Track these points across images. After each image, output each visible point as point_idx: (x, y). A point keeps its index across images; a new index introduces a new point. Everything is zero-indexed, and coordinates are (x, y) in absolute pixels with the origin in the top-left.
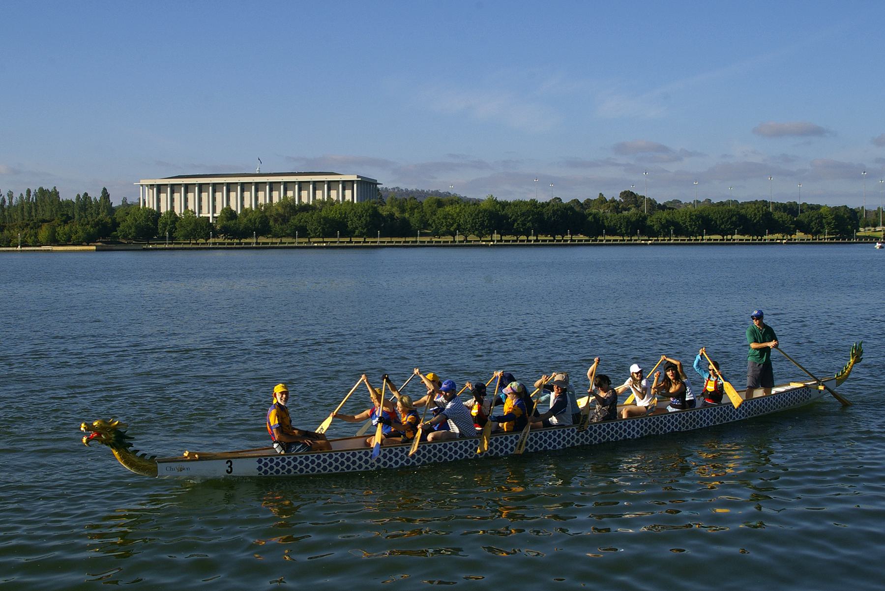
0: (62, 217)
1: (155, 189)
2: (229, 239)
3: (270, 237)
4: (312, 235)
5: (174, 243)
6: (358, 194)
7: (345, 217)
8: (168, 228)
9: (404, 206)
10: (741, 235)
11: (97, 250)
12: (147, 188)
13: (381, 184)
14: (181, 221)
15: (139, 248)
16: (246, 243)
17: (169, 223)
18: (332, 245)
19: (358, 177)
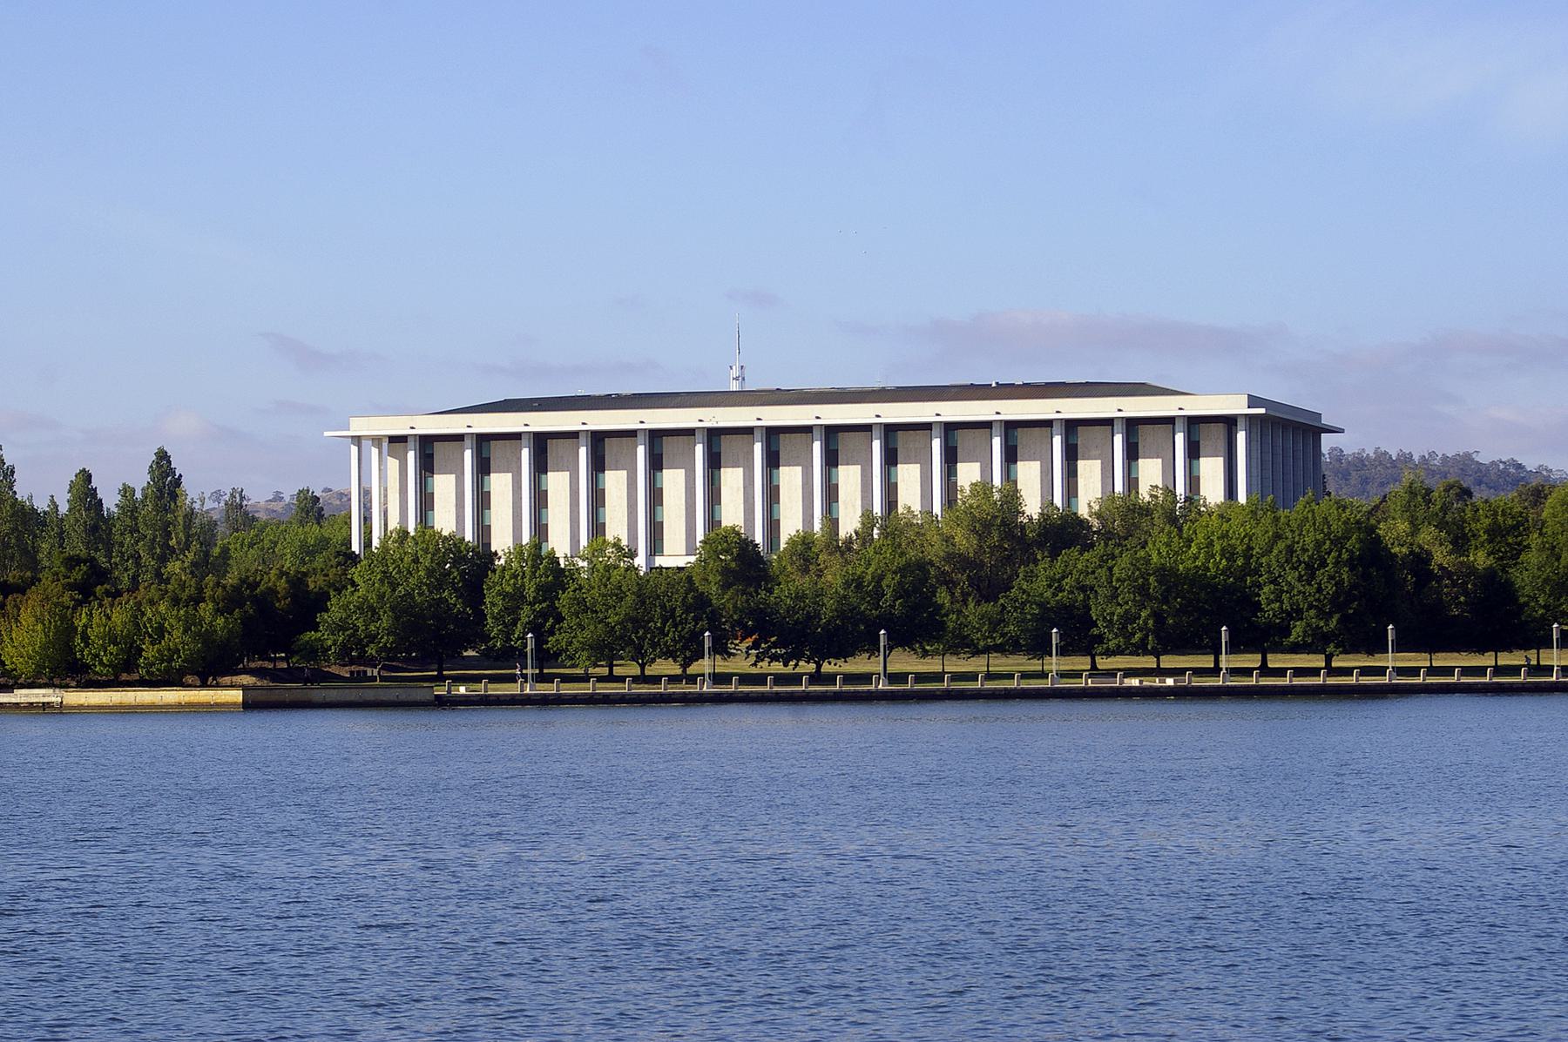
0: (71, 569)
1: (411, 456)
2: (774, 658)
3: (936, 653)
4: (1112, 644)
5: (449, 677)
6: (1254, 464)
7: (1246, 570)
8: (525, 614)
9: (1461, 524)
10: (1308, 654)
11: (248, 705)
12: (375, 451)
13: (1341, 431)
14: (581, 588)
15: (419, 694)
16: (849, 678)
17: (530, 592)
18: (1198, 682)
19: (1253, 401)
